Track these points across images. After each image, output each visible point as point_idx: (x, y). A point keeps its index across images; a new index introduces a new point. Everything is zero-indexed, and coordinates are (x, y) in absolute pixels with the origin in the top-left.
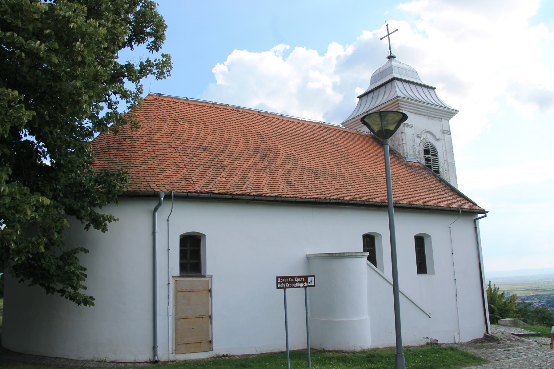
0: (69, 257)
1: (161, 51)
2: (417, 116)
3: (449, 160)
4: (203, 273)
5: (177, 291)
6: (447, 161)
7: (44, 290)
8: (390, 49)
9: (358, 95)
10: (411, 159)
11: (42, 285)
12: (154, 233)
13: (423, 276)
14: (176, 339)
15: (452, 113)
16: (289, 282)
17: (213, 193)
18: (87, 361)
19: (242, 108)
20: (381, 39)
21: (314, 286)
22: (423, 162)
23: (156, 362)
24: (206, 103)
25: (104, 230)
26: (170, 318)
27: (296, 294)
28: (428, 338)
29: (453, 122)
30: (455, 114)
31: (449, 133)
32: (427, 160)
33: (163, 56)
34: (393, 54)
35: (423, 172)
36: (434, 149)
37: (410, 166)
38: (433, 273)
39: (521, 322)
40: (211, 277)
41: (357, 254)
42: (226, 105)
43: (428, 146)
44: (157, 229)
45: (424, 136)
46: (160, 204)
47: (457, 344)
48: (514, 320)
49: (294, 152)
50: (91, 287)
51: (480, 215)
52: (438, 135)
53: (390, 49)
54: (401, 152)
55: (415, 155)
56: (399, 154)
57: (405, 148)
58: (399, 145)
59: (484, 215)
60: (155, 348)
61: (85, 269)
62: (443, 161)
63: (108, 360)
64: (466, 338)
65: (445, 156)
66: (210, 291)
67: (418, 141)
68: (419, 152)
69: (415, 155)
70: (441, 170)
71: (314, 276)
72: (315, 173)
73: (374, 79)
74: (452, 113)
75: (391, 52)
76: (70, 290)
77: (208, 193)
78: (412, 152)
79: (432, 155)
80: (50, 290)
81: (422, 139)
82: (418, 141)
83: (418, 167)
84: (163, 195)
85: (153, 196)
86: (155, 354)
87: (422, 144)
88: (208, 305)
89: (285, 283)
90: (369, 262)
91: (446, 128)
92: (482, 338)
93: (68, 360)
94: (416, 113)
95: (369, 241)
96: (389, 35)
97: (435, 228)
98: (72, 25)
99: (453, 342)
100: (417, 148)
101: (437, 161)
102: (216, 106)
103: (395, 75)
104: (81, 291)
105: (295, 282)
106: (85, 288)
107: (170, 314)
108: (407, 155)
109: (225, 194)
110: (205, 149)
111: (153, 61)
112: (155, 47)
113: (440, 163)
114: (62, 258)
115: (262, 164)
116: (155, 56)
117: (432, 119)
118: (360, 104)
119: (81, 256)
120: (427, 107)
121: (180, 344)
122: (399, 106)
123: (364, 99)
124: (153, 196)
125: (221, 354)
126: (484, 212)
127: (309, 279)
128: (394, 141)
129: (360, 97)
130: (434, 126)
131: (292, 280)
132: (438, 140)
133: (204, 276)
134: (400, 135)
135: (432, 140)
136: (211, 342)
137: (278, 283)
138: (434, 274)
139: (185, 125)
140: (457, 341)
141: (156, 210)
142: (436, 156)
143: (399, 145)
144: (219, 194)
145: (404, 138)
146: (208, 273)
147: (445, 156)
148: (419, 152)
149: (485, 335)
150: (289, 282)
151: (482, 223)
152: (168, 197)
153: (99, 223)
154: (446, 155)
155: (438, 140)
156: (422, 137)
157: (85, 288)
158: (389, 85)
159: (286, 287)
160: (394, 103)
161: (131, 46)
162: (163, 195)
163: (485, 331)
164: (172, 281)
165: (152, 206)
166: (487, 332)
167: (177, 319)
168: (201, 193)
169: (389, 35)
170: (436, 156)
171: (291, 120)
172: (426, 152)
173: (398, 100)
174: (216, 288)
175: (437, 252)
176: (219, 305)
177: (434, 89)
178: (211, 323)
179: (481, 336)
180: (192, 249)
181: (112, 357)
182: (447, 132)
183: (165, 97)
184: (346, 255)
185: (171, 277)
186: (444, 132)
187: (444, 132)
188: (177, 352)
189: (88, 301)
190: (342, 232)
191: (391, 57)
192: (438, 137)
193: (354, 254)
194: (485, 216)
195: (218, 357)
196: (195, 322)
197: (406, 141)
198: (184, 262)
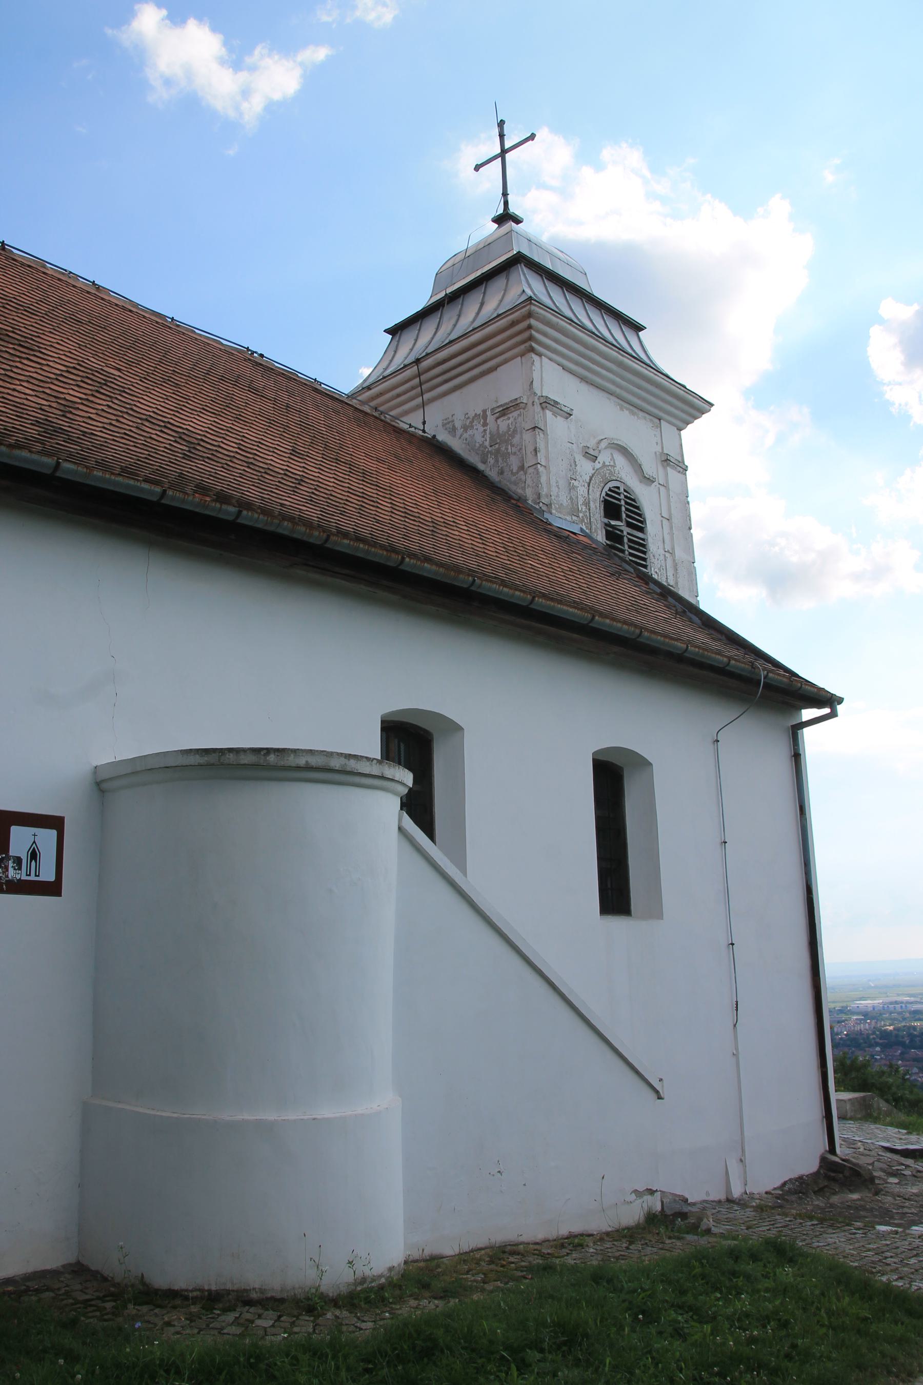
2: (584, 387)
3: (679, 553)
6: (672, 553)
8: (505, 194)
9: (391, 324)
10: (560, 520)
13: (616, 923)
21: (53, 889)
28: (651, 1192)
29: (695, 439)
30: (702, 412)
32: (613, 536)
34: (512, 209)
37: (562, 537)
38: (655, 912)
39: (884, 1106)
41: (352, 765)
43: (615, 490)
47: (741, 1203)
48: (864, 1098)
51: (808, 714)
52: (650, 467)
53: (505, 194)
54: (529, 494)
56: (522, 499)
57: (543, 479)
58: (522, 468)
59: (827, 711)
62: (661, 551)
64: (766, 1177)
65: (667, 538)
67: (586, 468)
68: (587, 504)
69: (575, 512)
71: (55, 823)
75: (506, 203)
78: (564, 499)
79: (629, 525)
81: (597, 465)
82: (586, 468)
87: (597, 480)
90: (409, 824)
92: (816, 1174)
94: (583, 379)
95: (411, 741)
96: (504, 152)
97: (664, 730)
99: (722, 1197)
100: (582, 490)
108: (549, 506)
113: (649, 556)
117: (633, 414)
118: (393, 349)
120: (620, 365)
122: (531, 338)
126: (828, 701)
128: (506, 456)
129: (395, 331)
130: (639, 435)
132: (648, 480)
134: (527, 436)
138: (660, 916)
140: (737, 1192)
142: (641, 530)
143: (522, 468)
145: (541, 445)
147: (667, 538)
148: (587, 504)
149: (823, 1160)
151: (814, 739)
154: (671, 534)
155: (648, 480)
156: (600, 459)
160: (513, 324)
163: (824, 1145)
166: (832, 1150)
169: (504, 152)
170: (641, 530)
172: (611, 509)
173: (530, 315)
179: (809, 1165)
182: (675, 464)
184: (292, 760)
186: (666, 461)
191: (505, 218)
193: (336, 763)
194: (833, 715)
197: (547, 458)
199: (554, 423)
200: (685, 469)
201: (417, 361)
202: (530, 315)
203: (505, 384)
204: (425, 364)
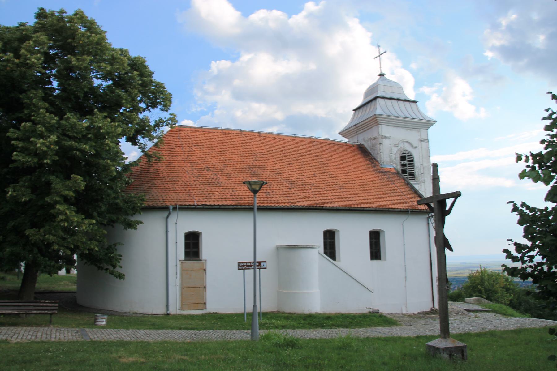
0: (111, 249)
1: (170, 112)
2: (395, 128)
4: (200, 259)
5: (183, 270)
7: (96, 268)
11: (96, 265)
12: (167, 232)
13: (376, 262)
14: (182, 301)
15: (429, 124)
16: (247, 266)
17: (206, 205)
18: (126, 313)
19: (245, 131)
20: (386, 52)
22: (399, 168)
23: (168, 314)
24: (217, 129)
25: (135, 229)
26: (178, 287)
27: (249, 273)
31: (427, 140)
32: (403, 165)
33: (171, 115)
35: (395, 177)
36: (411, 156)
37: (383, 172)
38: (385, 260)
40: (206, 260)
42: (232, 130)
44: (169, 229)
45: (401, 145)
46: (170, 214)
49: (279, 167)
50: (124, 267)
54: (379, 160)
55: (391, 161)
60: (167, 306)
61: (121, 256)
63: (139, 312)
66: (205, 270)
67: (395, 149)
69: (391, 161)
70: (416, 173)
71: (265, 262)
72: (292, 184)
73: (367, 94)
74: (429, 124)
76: (111, 268)
77: (202, 205)
78: (388, 160)
80: (100, 268)
82: (395, 149)
83: (392, 173)
84: (171, 208)
85: (166, 208)
86: (168, 310)
88: (203, 279)
89: (244, 266)
91: (423, 137)
93: (114, 311)
98: (102, 131)
101: (413, 166)
102: (224, 131)
103: (379, 94)
104: (118, 269)
105: (251, 266)
106: (121, 267)
107: (178, 284)
109: (215, 205)
110: (208, 170)
111: (163, 119)
112: (166, 109)
114: (107, 249)
115: (261, 176)
116: (165, 116)
119: (118, 247)
121: (184, 305)
123: (357, 112)
124: (166, 208)
125: (212, 312)
127: (262, 264)
129: (355, 110)
130: (412, 136)
131: (249, 264)
132: (415, 148)
133: (201, 260)
135: (408, 148)
136: (205, 304)
137: (239, 266)
139: (197, 150)
141: (168, 217)
144: (211, 205)
146: (204, 258)
148: (395, 159)
150: (247, 266)
152: (175, 208)
153: (131, 225)
155: (415, 148)
157: (121, 267)
158: (373, 103)
159: (244, 269)
161: (149, 110)
162: (171, 208)
163: (432, 306)
164: (179, 263)
165: (165, 214)
166: (434, 307)
167: (183, 288)
168: (198, 205)
170: (412, 161)
171: (285, 138)
172: (403, 158)
173: (376, 117)
174: (209, 267)
175: (389, 244)
176: (210, 279)
177: (416, 102)
178: (205, 291)
180: (193, 242)
181: (141, 311)
183: (185, 127)
185: (178, 261)
186: (421, 141)
187: (421, 141)
188: (182, 309)
189: (121, 276)
190: (307, 230)
192: (415, 145)
195: (210, 313)
196: (194, 290)
198: (188, 250)
199: (386, 142)
200: (428, 141)
201: (356, 125)
202: (376, 117)
203: (372, 133)
204: (358, 125)
